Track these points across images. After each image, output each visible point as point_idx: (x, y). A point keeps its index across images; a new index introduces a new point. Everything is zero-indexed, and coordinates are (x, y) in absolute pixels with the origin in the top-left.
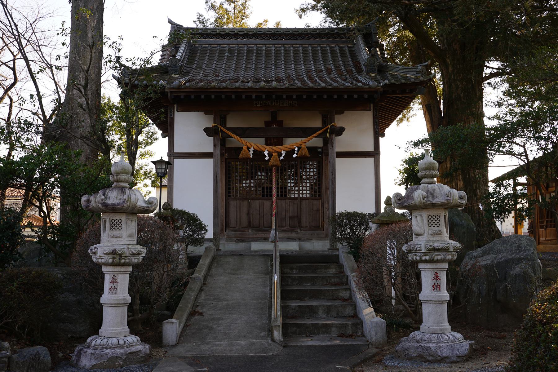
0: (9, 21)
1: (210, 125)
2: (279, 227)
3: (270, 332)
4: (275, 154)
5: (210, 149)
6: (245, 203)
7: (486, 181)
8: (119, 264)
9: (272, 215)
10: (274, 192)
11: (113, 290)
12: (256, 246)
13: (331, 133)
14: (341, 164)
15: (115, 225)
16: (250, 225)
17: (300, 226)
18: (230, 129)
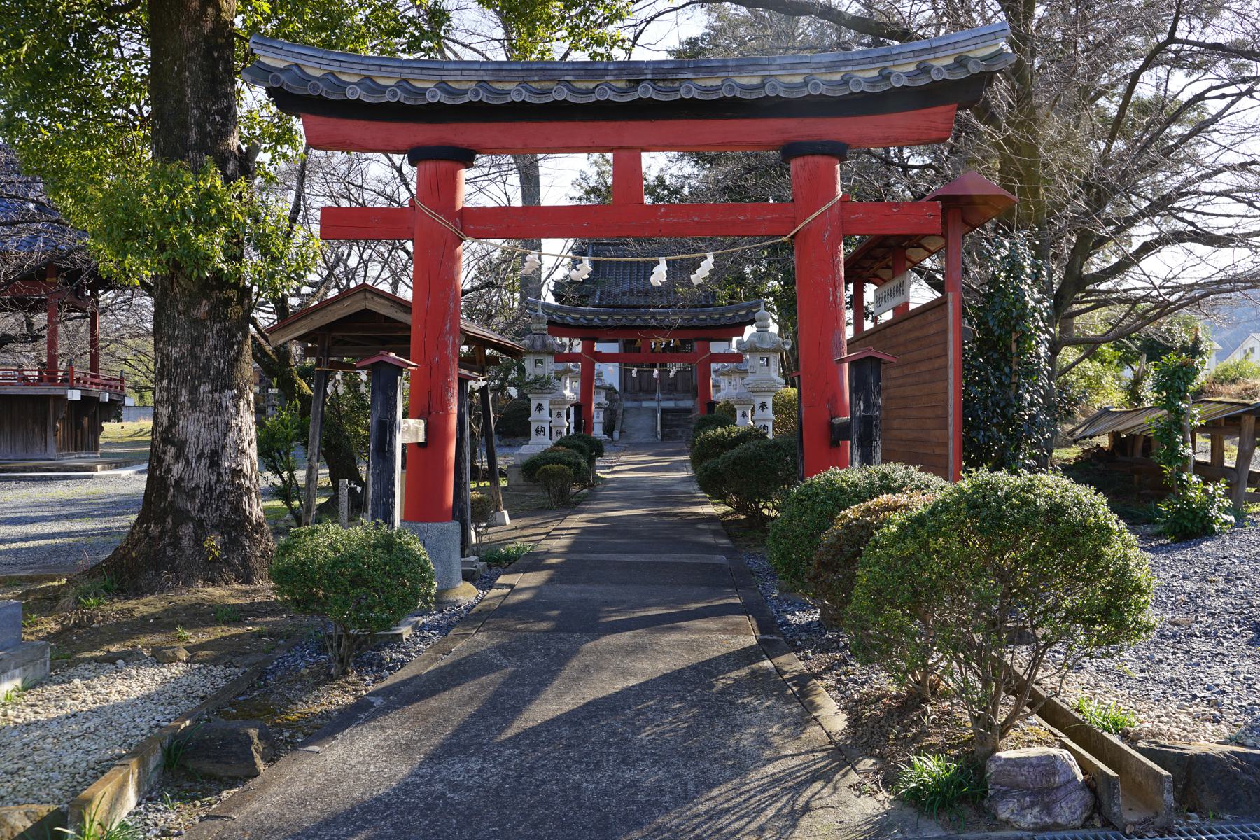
0: (568, 529)
7: (351, 208)
12: (645, 404)
15: (599, 393)
16: (641, 390)
17: (676, 389)
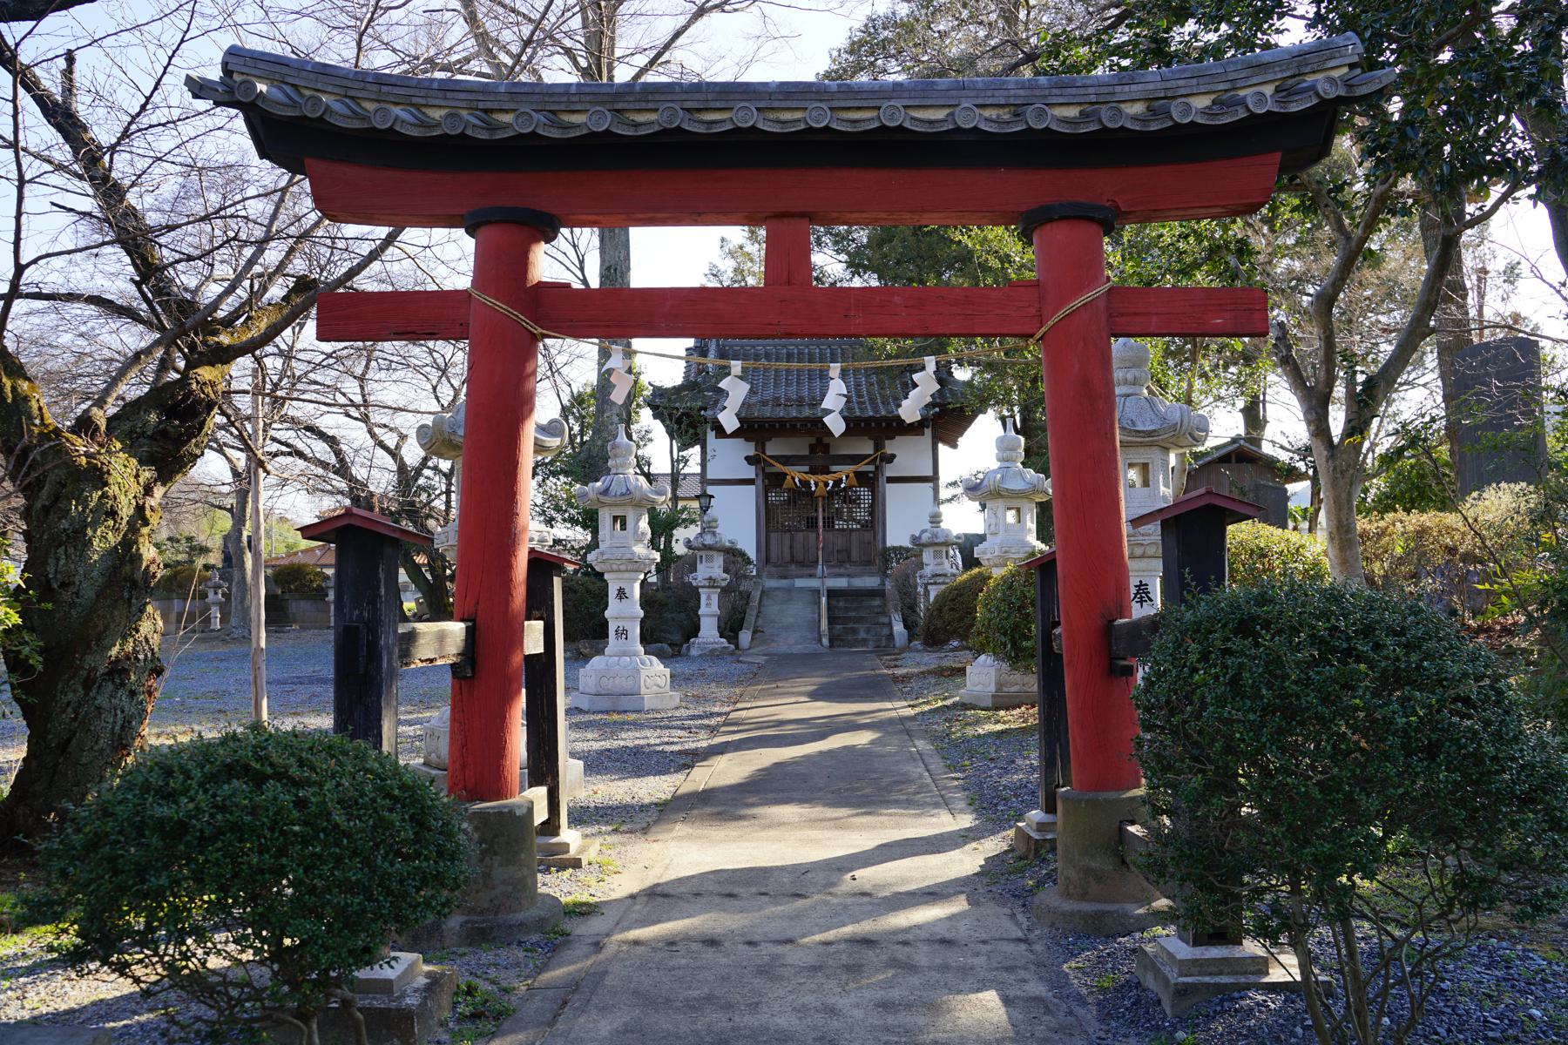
1: (752, 452)
2: (826, 561)
3: (820, 641)
4: (821, 484)
5: (753, 476)
6: (787, 536)
8: (713, 587)
9: (818, 549)
10: (821, 524)
11: (708, 605)
12: (799, 583)
13: (881, 461)
14: (893, 493)
16: (793, 560)
17: (849, 560)
18: (770, 457)
